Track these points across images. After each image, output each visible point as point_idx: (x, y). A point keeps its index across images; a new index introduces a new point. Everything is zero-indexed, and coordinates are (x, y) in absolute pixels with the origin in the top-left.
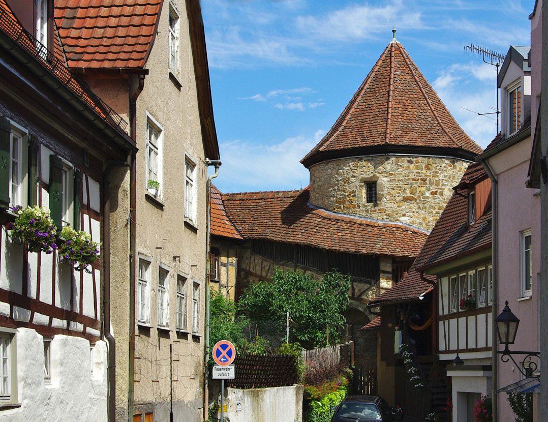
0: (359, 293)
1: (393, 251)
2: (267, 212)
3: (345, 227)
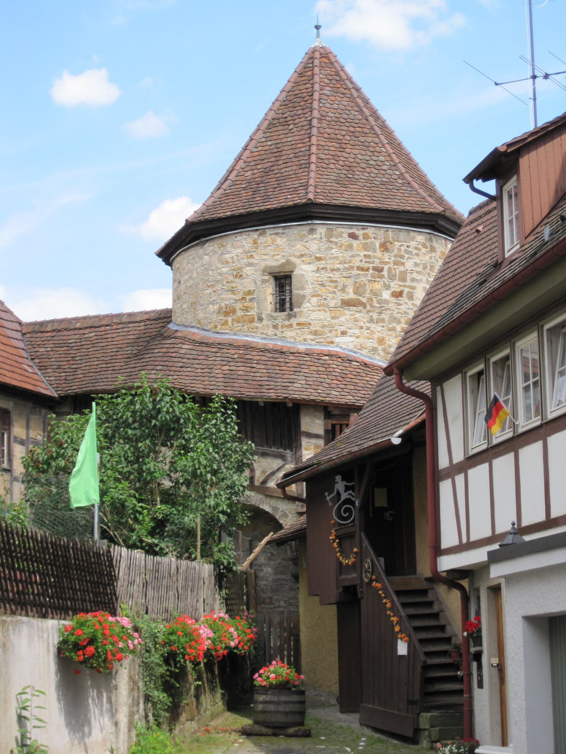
1: (325, 395)
3: (236, 356)
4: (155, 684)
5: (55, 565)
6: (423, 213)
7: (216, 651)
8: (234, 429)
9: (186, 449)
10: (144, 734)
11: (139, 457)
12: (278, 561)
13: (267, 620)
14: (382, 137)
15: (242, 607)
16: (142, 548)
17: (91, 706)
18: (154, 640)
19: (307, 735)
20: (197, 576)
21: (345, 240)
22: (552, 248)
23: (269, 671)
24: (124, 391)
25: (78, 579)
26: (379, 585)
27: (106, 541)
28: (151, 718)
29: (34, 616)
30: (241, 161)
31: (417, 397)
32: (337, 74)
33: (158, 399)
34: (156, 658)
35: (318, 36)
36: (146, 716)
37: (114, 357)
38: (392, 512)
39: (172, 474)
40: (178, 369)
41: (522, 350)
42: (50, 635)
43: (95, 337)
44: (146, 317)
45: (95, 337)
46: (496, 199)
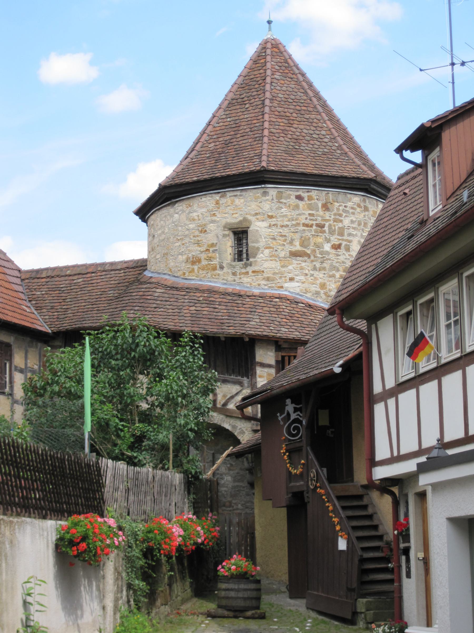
0: (224, 401)
1: (276, 332)
3: (201, 299)
4: (135, 575)
5: (53, 474)
6: (358, 178)
7: (186, 547)
8: (200, 360)
9: (160, 376)
10: (127, 616)
11: (119, 384)
12: (236, 471)
13: (227, 521)
14: (324, 115)
15: (206, 510)
16: (123, 460)
17: (83, 593)
18: (135, 538)
19: (262, 617)
20: (169, 484)
21: (293, 201)
22: (471, 208)
23: (230, 564)
24: (108, 328)
25: (72, 486)
26: (322, 491)
27: (95, 454)
28: (132, 602)
29: (35, 518)
30: (205, 135)
31: (355, 333)
32: (286, 62)
33: (137, 335)
34: (136, 552)
35: (270, 29)
36: (129, 601)
37: (98, 299)
38: (333, 430)
39: (148, 398)
40: (153, 309)
41: (444, 294)
42: (50, 533)
43: (83, 283)
44: (125, 265)
45: (83, 283)
46: (422, 166)
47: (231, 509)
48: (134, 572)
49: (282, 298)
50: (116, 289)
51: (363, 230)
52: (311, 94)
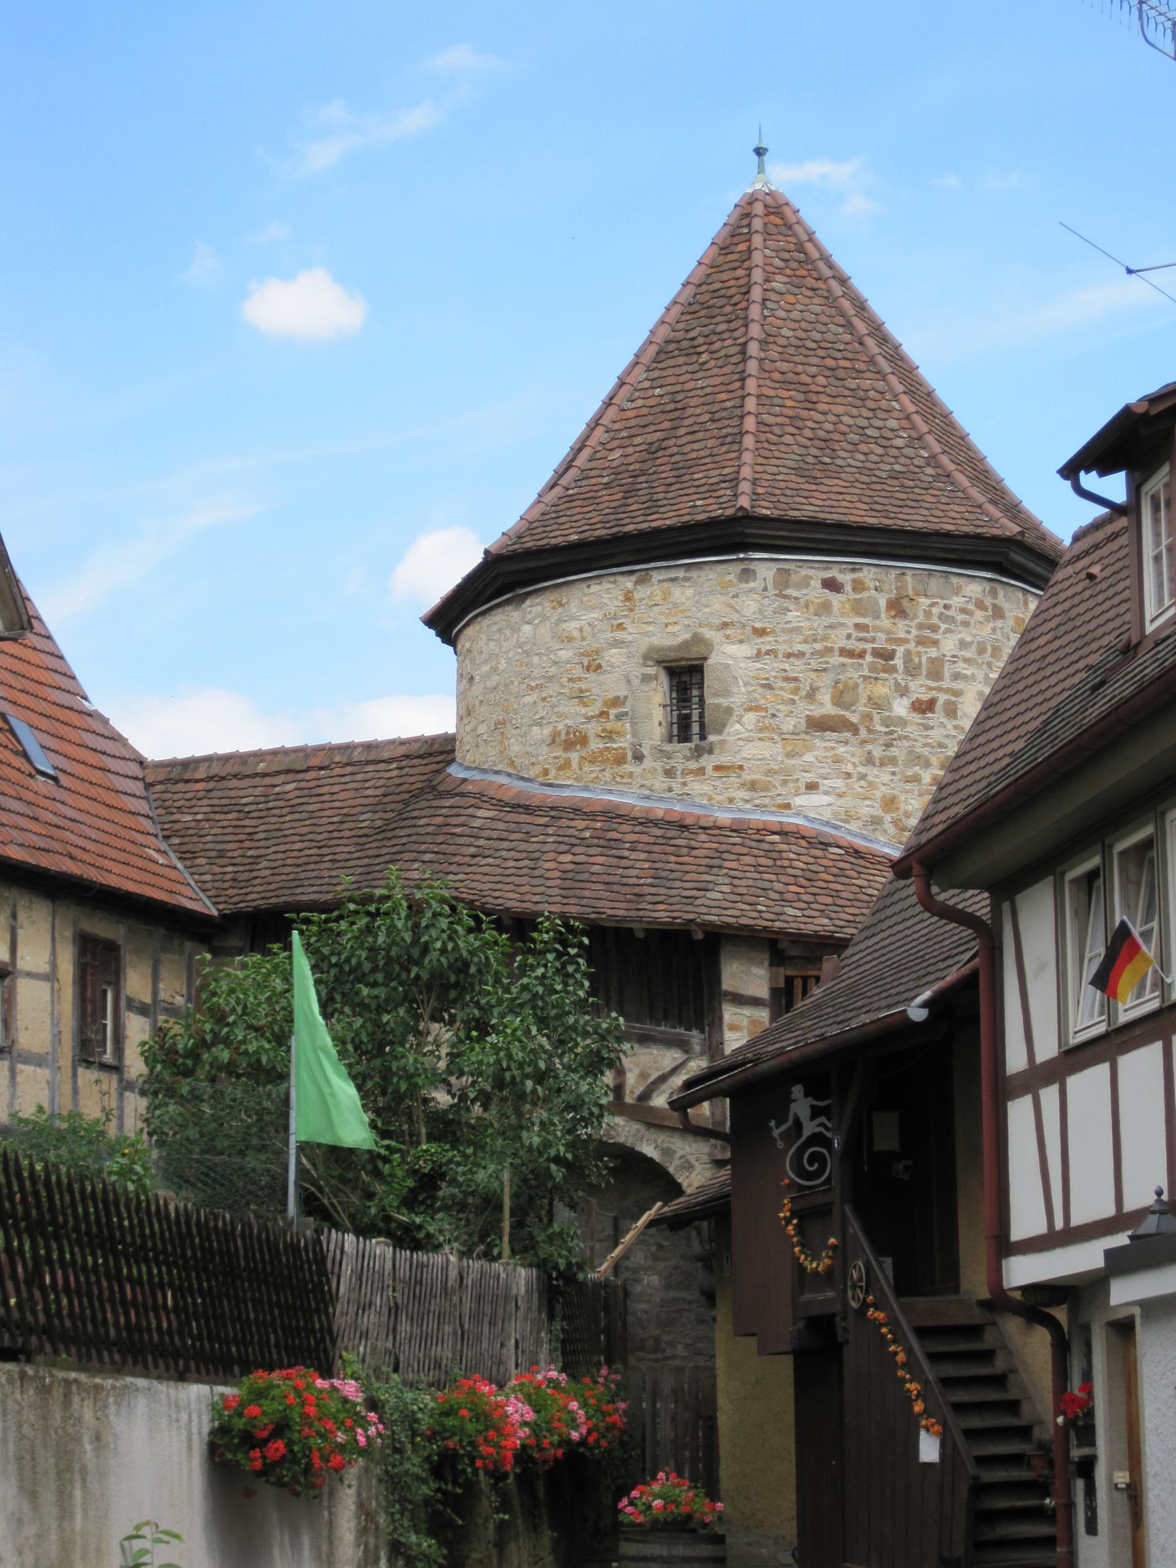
0: (641, 1089)
1: (772, 917)
2: (305, 815)
3: (587, 834)
4: (412, 1519)
6: (978, 536)
7: (541, 1450)
8: (582, 986)
9: (483, 1028)
14: (893, 380)
15: (595, 1358)
18: (411, 1428)
21: (816, 592)
24: (352, 906)
26: (880, 1315)
30: (600, 429)
32: (801, 249)
34: (414, 1465)
35: (761, 169)
37: (335, 834)
38: (910, 1162)
39: (453, 1080)
40: (467, 860)
42: (194, 1416)
43: (297, 793)
44: (402, 750)
45: (297, 793)
46: (1128, 511)
47: (659, 1356)
48: (407, 1514)
49: (786, 833)
50: (380, 807)
51: (989, 665)
52: (861, 327)
